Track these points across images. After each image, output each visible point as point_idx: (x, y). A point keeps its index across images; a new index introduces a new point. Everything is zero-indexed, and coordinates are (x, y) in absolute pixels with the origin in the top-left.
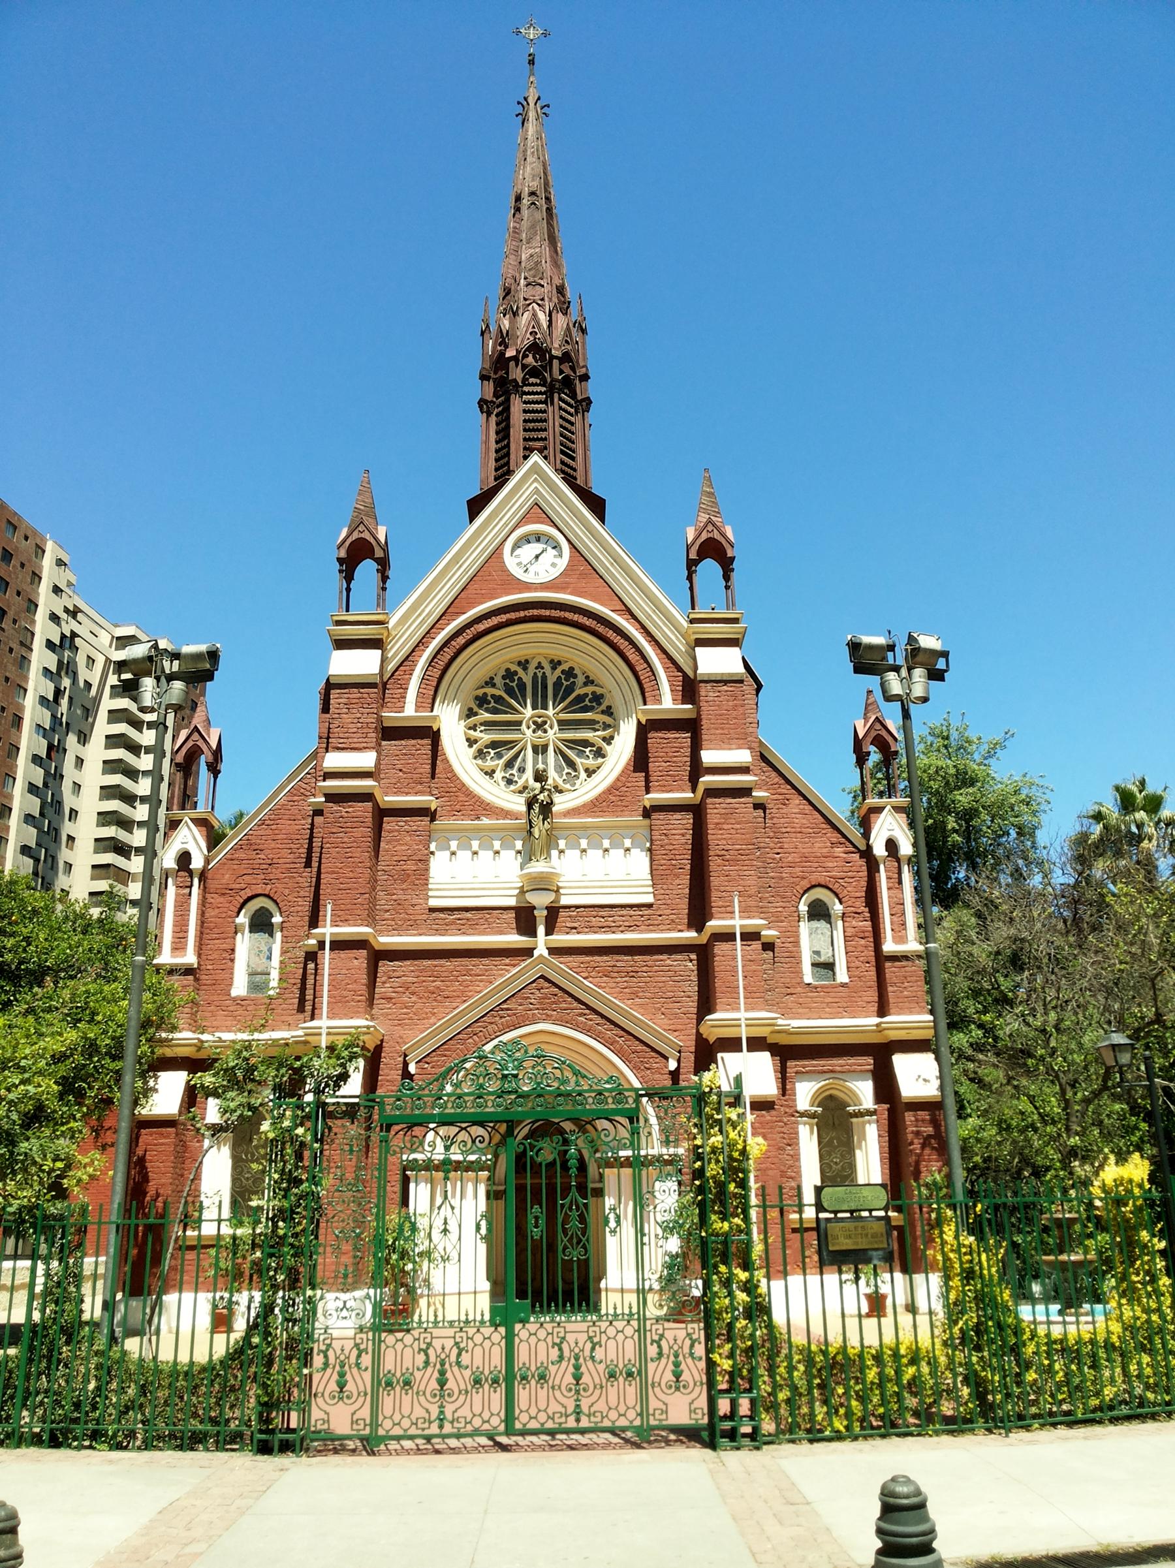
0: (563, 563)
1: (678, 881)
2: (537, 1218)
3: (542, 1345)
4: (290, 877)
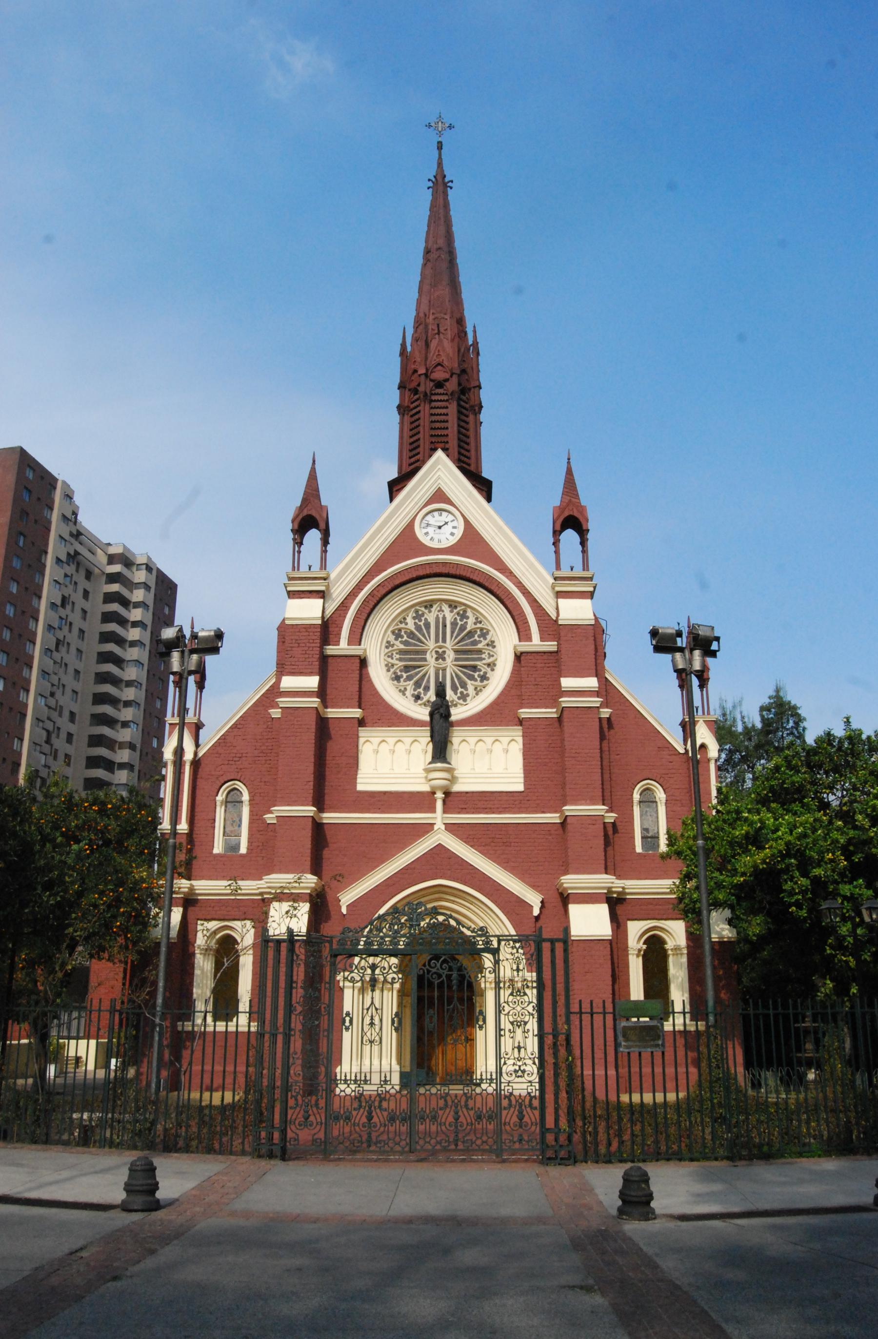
0: (459, 533)
2: (431, 1018)
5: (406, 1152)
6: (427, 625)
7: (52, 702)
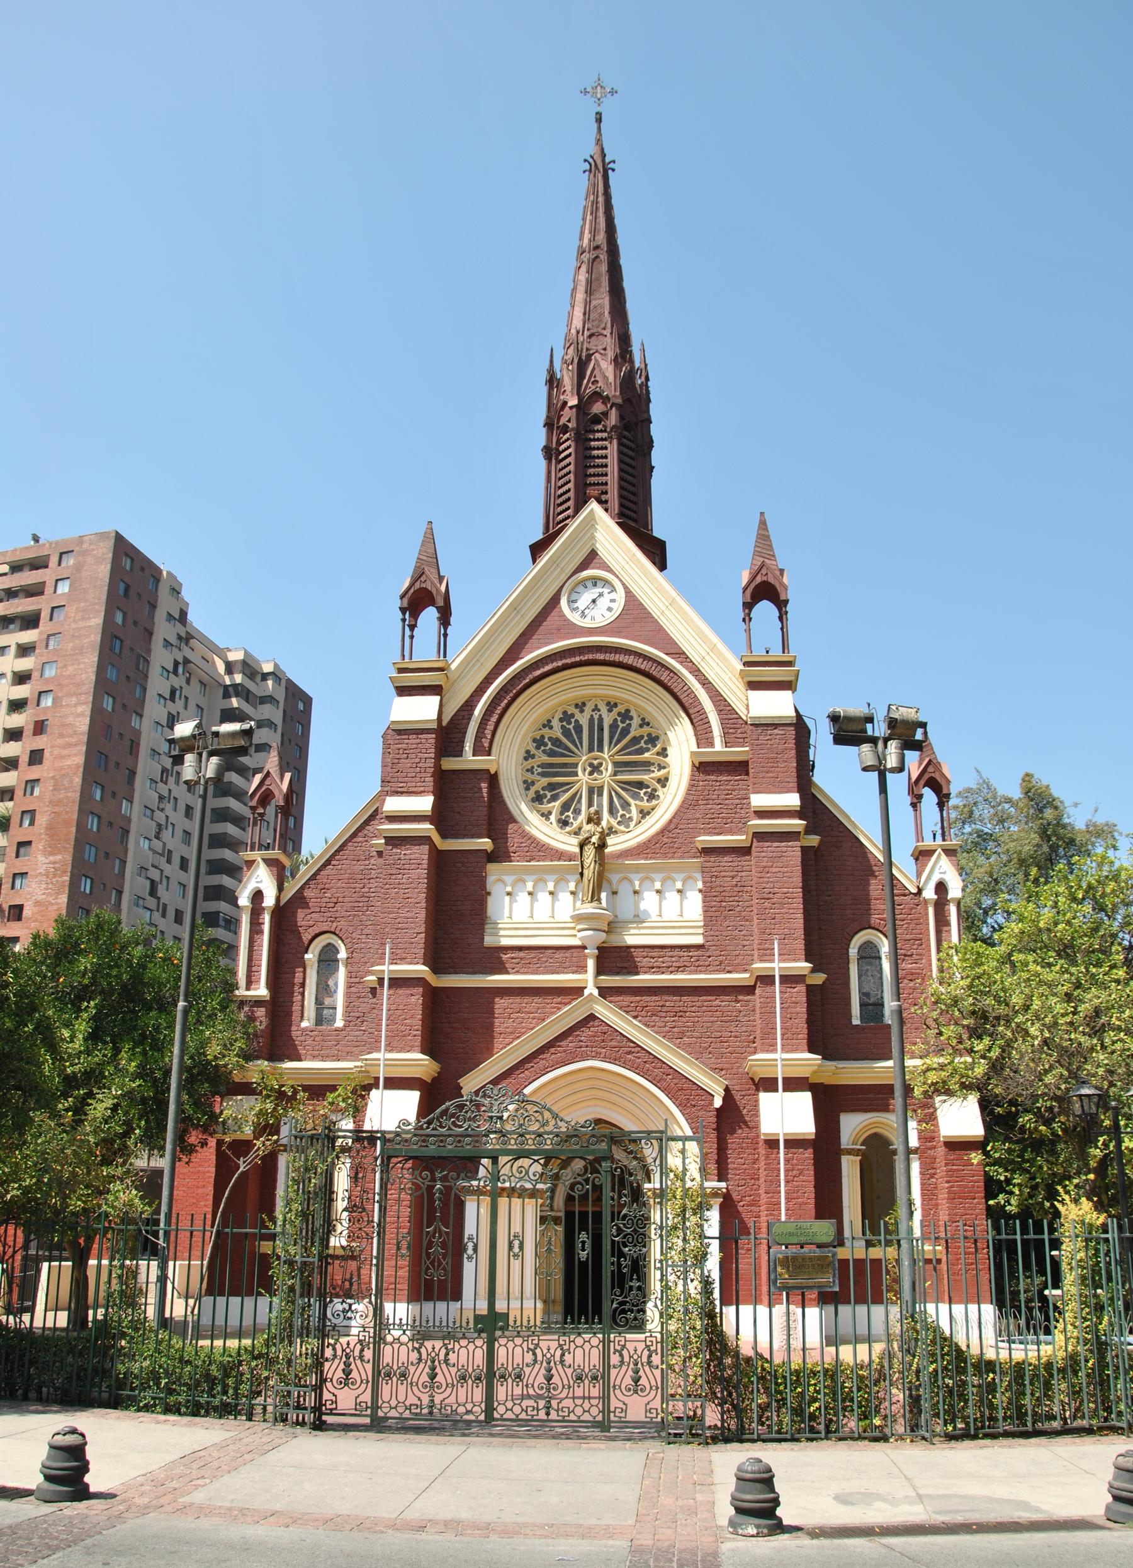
0: (618, 607)
1: (727, 923)
3: (518, 1350)
5: (481, 1422)
6: (579, 728)
7: (158, 845)
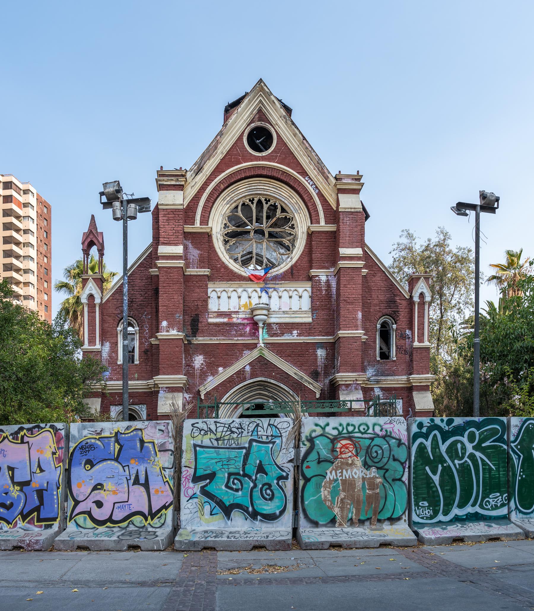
4: (141, 308)
